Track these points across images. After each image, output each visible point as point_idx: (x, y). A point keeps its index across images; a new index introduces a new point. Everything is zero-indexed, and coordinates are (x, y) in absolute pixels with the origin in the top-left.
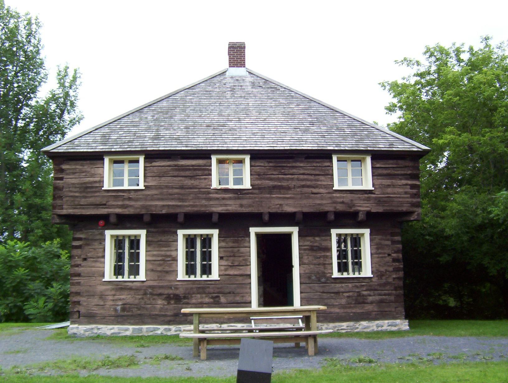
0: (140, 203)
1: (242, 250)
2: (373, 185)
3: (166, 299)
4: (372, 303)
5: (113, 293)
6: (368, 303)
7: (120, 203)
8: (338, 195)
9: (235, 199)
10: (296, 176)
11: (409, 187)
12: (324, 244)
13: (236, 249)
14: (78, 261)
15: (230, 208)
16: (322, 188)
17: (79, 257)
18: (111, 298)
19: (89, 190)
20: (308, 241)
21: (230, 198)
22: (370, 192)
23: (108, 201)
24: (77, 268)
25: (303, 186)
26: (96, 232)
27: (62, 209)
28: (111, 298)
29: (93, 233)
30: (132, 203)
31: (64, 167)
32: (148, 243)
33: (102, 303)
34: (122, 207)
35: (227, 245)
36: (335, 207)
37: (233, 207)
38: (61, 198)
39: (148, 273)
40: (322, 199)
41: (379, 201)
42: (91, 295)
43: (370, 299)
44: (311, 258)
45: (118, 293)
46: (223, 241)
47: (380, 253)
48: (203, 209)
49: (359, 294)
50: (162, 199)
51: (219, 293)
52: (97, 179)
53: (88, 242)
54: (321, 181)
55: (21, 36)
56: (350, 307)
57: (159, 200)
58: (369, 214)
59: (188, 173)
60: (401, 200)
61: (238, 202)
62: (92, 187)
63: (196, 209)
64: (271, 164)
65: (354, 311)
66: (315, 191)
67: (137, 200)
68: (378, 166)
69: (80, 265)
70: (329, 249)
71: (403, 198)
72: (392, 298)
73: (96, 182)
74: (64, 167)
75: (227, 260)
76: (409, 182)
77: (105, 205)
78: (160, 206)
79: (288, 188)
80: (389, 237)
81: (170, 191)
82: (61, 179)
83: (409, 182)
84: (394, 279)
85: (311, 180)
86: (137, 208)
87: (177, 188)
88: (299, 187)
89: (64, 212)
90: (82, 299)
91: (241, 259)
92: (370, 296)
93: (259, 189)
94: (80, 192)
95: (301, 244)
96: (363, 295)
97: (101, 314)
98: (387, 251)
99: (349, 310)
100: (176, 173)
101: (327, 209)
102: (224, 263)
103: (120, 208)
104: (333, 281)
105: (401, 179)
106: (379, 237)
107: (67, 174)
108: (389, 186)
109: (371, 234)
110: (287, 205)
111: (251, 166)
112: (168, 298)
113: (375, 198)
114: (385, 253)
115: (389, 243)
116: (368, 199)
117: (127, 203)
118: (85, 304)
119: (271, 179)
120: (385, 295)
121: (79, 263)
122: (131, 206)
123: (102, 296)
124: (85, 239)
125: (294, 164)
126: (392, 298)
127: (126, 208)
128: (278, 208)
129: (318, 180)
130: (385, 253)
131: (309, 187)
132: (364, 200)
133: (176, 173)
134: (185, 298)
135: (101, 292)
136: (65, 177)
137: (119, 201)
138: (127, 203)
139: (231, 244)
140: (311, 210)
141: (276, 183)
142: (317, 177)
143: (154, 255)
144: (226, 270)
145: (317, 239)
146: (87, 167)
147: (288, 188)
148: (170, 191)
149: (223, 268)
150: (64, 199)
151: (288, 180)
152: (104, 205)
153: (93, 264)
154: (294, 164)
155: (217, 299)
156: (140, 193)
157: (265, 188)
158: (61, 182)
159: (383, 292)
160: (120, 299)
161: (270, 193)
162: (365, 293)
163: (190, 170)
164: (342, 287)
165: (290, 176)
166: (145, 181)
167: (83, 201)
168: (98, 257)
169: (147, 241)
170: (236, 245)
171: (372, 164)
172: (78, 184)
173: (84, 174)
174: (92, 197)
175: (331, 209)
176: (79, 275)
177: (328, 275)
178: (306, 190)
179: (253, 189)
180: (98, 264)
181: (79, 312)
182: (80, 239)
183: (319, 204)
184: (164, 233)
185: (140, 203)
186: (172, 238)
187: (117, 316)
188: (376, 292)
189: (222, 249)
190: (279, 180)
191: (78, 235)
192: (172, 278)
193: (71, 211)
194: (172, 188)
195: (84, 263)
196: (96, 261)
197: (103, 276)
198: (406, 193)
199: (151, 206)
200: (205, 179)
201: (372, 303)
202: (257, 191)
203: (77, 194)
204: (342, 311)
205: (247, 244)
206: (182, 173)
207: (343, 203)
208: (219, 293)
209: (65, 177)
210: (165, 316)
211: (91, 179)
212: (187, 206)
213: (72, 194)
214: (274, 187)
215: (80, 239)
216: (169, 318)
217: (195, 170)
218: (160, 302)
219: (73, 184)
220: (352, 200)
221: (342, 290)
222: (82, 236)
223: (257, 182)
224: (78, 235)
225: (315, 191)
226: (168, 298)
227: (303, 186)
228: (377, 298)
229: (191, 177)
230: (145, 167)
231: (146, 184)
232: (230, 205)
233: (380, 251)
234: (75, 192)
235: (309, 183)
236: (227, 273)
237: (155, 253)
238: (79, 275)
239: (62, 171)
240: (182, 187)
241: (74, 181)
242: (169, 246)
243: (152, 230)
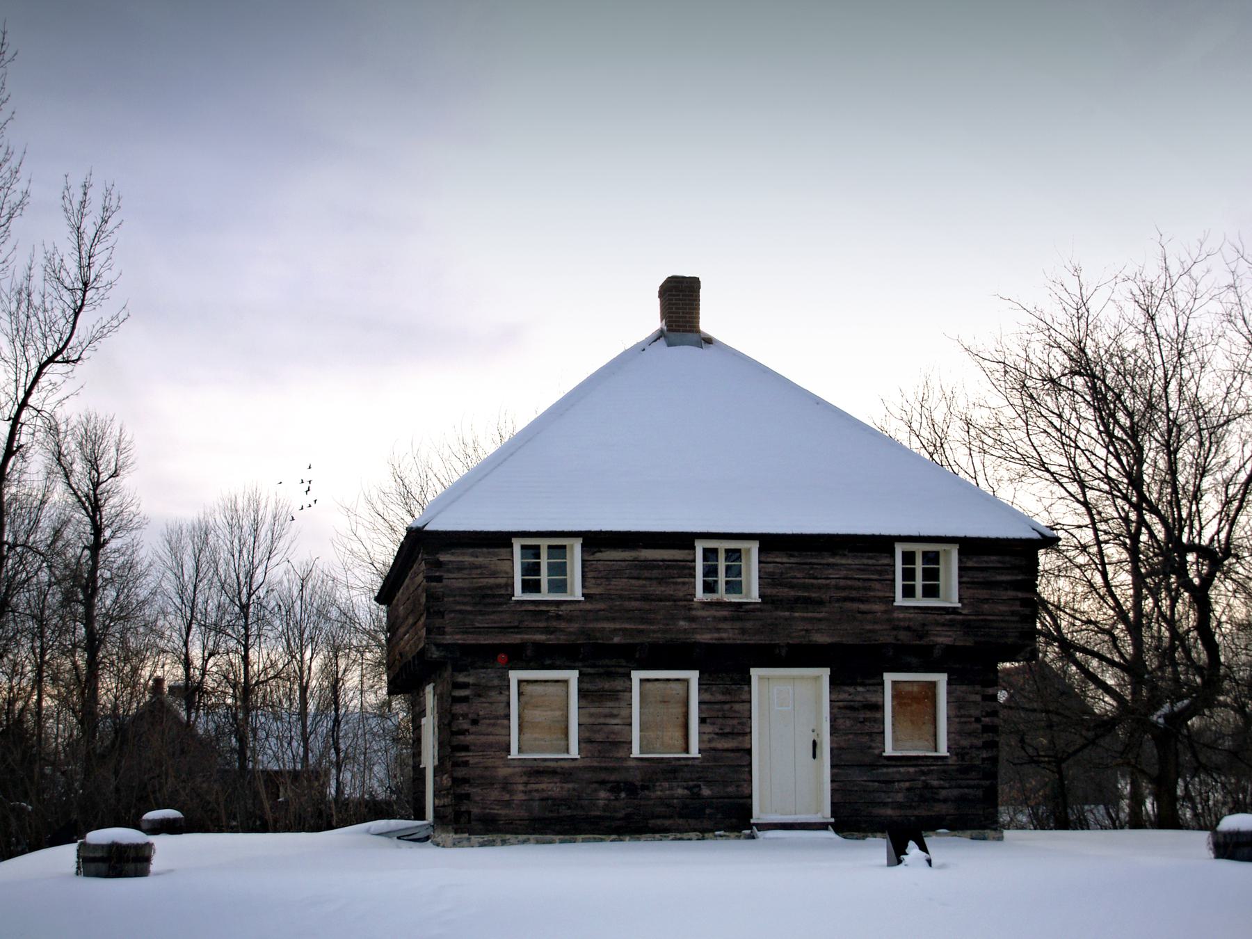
0: (574, 626)
1: (737, 707)
2: (960, 600)
3: (611, 790)
4: (945, 801)
5: (525, 779)
6: (939, 800)
7: (541, 625)
8: (901, 616)
9: (732, 619)
10: (833, 582)
11: (1018, 603)
12: (874, 698)
13: (727, 707)
14: (465, 725)
15: (724, 635)
16: (875, 602)
17: (465, 716)
18: (521, 787)
19: (488, 600)
20: (845, 692)
21: (725, 619)
22: (954, 611)
23: (521, 622)
24: (462, 737)
25: (845, 599)
26: (491, 673)
27: (444, 633)
28: (521, 787)
29: (486, 675)
30: (563, 625)
31: (444, 557)
32: (582, 694)
33: (507, 797)
34: (547, 631)
35: (713, 699)
36: (896, 638)
37: (729, 634)
38: (441, 614)
39: (583, 745)
40: (875, 623)
41: (967, 627)
42: (490, 783)
43: (944, 793)
44: (848, 723)
45: (532, 780)
46: (706, 690)
47: (961, 716)
48: (682, 636)
49: (926, 786)
50: (614, 619)
51: (698, 779)
52: (502, 581)
53: (481, 691)
54: (874, 590)
55: (1009, 745)
56: (910, 807)
57: (607, 619)
58: (949, 649)
59: (655, 573)
60: (1004, 625)
61: (738, 625)
62: (494, 596)
63: (668, 636)
64: (793, 560)
65: (916, 813)
66: (863, 607)
67: (570, 619)
68: (970, 564)
69: (467, 731)
70: (879, 708)
71: (1007, 621)
72: (980, 793)
73: (499, 586)
74: (444, 557)
75: (713, 724)
76: (1020, 595)
77: (517, 627)
78: (614, 631)
79: (821, 603)
80: (978, 688)
81: (627, 604)
82: (439, 579)
83: (1020, 595)
84: (983, 759)
85: (858, 589)
86: (571, 633)
87: (636, 600)
88: (838, 600)
89: (448, 639)
90: (472, 790)
91: (735, 722)
92: (944, 788)
93: (773, 602)
94: (475, 604)
95: (834, 697)
96: (932, 787)
97: (506, 815)
98: (975, 712)
99: (909, 812)
100: (635, 573)
101: (882, 640)
102: (708, 728)
103: (542, 633)
104: (886, 762)
105: (1006, 589)
106: (964, 688)
107: (449, 571)
108: (986, 601)
109: (949, 683)
110: (818, 631)
111: (760, 562)
112: (615, 788)
113: (962, 623)
114: (970, 716)
115: (978, 698)
116: (951, 624)
117: (554, 624)
118: (478, 799)
119: (792, 587)
120: (968, 787)
121: (466, 727)
122: (561, 630)
123: (506, 785)
124: (474, 685)
125: (831, 560)
126: (980, 793)
127: (551, 633)
128: (804, 637)
129: (870, 589)
130: (970, 716)
131: (853, 600)
132: (943, 625)
133: (635, 573)
134: (644, 788)
135: (505, 778)
136: (446, 575)
137: (540, 621)
138: (554, 624)
139: (720, 697)
140: (857, 641)
141: (800, 594)
142: (867, 584)
143: (591, 715)
144: (710, 741)
145: (860, 689)
146: (482, 558)
147: (821, 603)
148: (627, 604)
149: (706, 737)
150: (446, 617)
151: (820, 587)
152: (517, 629)
153: (490, 729)
154: (831, 560)
155: (695, 790)
156: (577, 607)
157: (781, 601)
158: (440, 585)
159: (964, 783)
160: (537, 791)
161: (792, 609)
162: (935, 783)
163: (659, 567)
164: (899, 772)
165: (824, 582)
166: (583, 587)
167: (480, 621)
168: (497, 718)
169: (580, 690)
170: (728, 698)
171: (960, 561)
172: (469, 589)
173: (479, 571)
174: (494, 612)
175: (890, 640)
176: (466, 748)
177: (877, 752)
178: (848, 605)
179: (764, 602)
180: (498, 730)
181: (469, 813)
182: (465, 686)
183: (870, 631)
184: (610, 675)
185: (574, 626)
186: (619, 684)
187: (534, 820)
188: (953, 783)
189: (704, 707)
190: (805, 587)
191: (461, 678)
192: (621, 754)
193: (459, 639)
194: (630, 599)
195: (473, 729)
196: (494, 725)
197: (509, 752)
198: (1013, 613)
199: (593, 630)
200: (684, 583)
201: (945, 801)
202: (769, 607)
203: (469, 608)
204: (897, 813)
205: (744, 697)
206: (646, 574)
207: (908, 629)
208: (698, 779)
209: (446, 575)
210: (612, 819)
211: (492, 581)
212: (654, 632)
213: (458, 608)
214: (797, 600)
215: (465, 686)
216: (618, 823)
217: (668, 567)
218: (603, 794)
219: (462, 589)
220: (924, 625)
221: (898, 777)
222: (471, 680)
223: (769, 591)
224: (461, 678)
225: (863, 607)
226: (615, 788)
227: (845, 599)
228: (956, 792)
229: (661, 581)
230: (583, 561)
231: (586, 591)
232: (725, 630)
233: (963, 712)
234: (464, 604)
235: (854, 594)
236: (713, 745)
237: (593, 710)
238: (466, 748)
239: (440, 564)
240: (646, 598)
241: (460, 584)
242: (617, 699)
243: (590, 670)
